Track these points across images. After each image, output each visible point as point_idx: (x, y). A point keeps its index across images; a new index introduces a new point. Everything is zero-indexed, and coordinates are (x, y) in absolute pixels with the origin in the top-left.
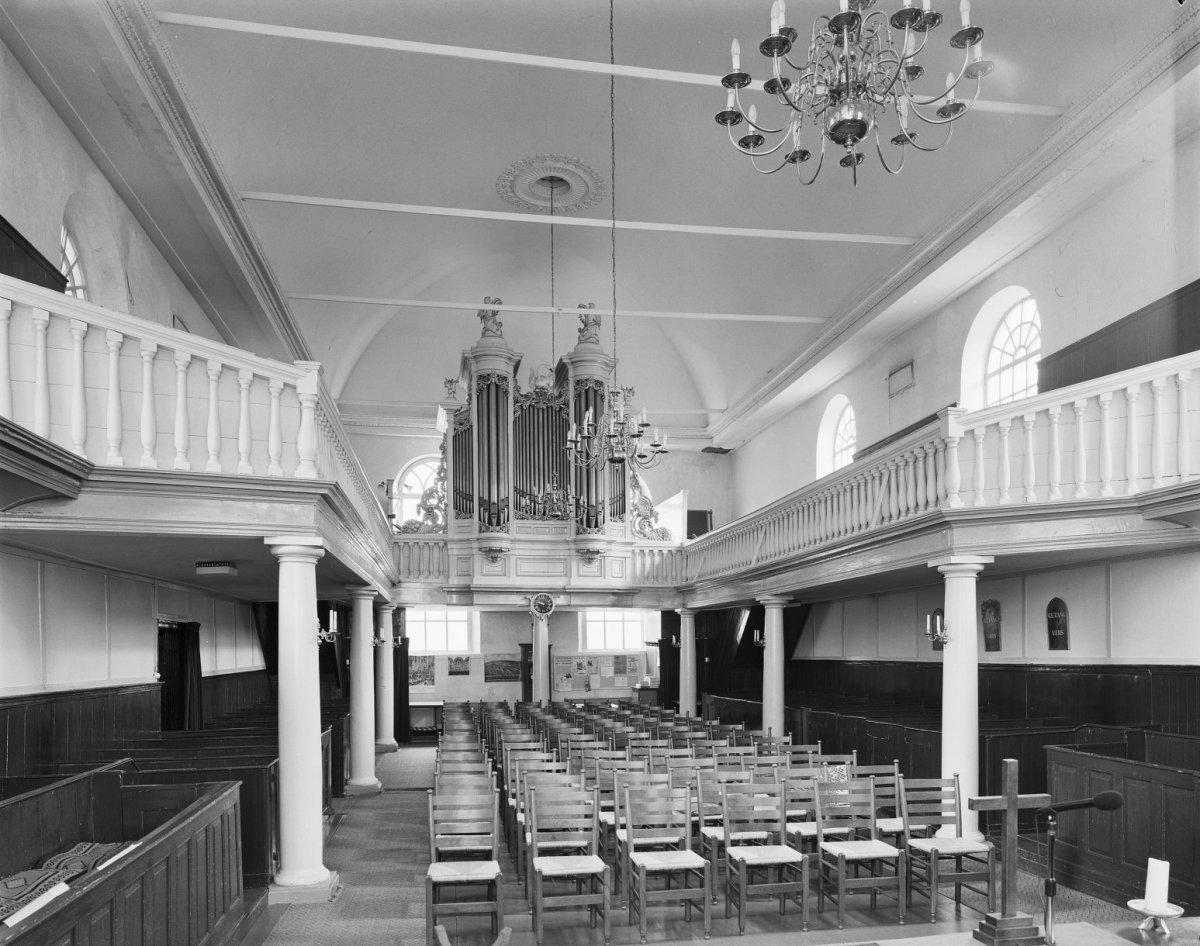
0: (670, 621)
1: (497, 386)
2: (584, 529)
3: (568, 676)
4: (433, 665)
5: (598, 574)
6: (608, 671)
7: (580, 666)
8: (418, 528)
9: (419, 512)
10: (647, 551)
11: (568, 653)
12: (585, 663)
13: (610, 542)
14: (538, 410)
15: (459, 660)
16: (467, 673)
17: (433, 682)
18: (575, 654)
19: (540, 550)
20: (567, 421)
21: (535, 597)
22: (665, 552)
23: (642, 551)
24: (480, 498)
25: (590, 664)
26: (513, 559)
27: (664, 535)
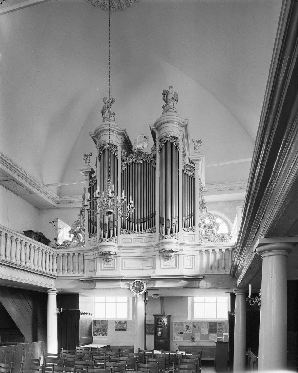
3: (181, 333)
4: (107, 325)
5: (174, 266)
6: (206, 331)
7: (188, 327)
8: (69, 245)
9: (70, 236)
10: (210, 250)
11: (181, 320)
12: (191, 326)
13: (182, 244)
14: (138, 164)
15: (120, 323)
16: (124, 330)
17: (106, 334)
18: (186, 321)
20: (155, 168)
21: (132, 283)
22: (224, 250)
23: (207, 250)
25: (194, 326)
26: (120, 259)
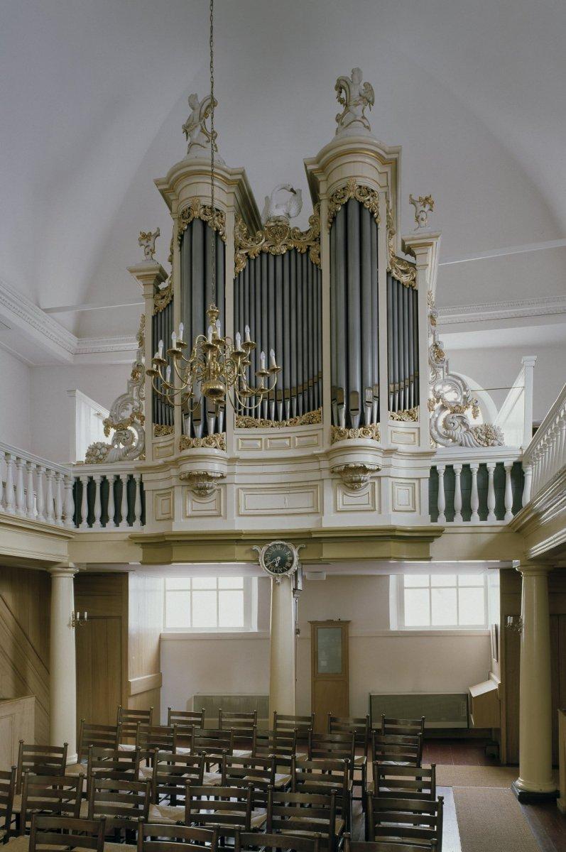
0: (510, 581)
1: (205, 224)
2: (340, 432)
5: (369, 507)
9: (107, 433)
13: (389, 452)
19: (275, 473)
21: (265, 548)
24: (332, 387)
27: (488, 436)
